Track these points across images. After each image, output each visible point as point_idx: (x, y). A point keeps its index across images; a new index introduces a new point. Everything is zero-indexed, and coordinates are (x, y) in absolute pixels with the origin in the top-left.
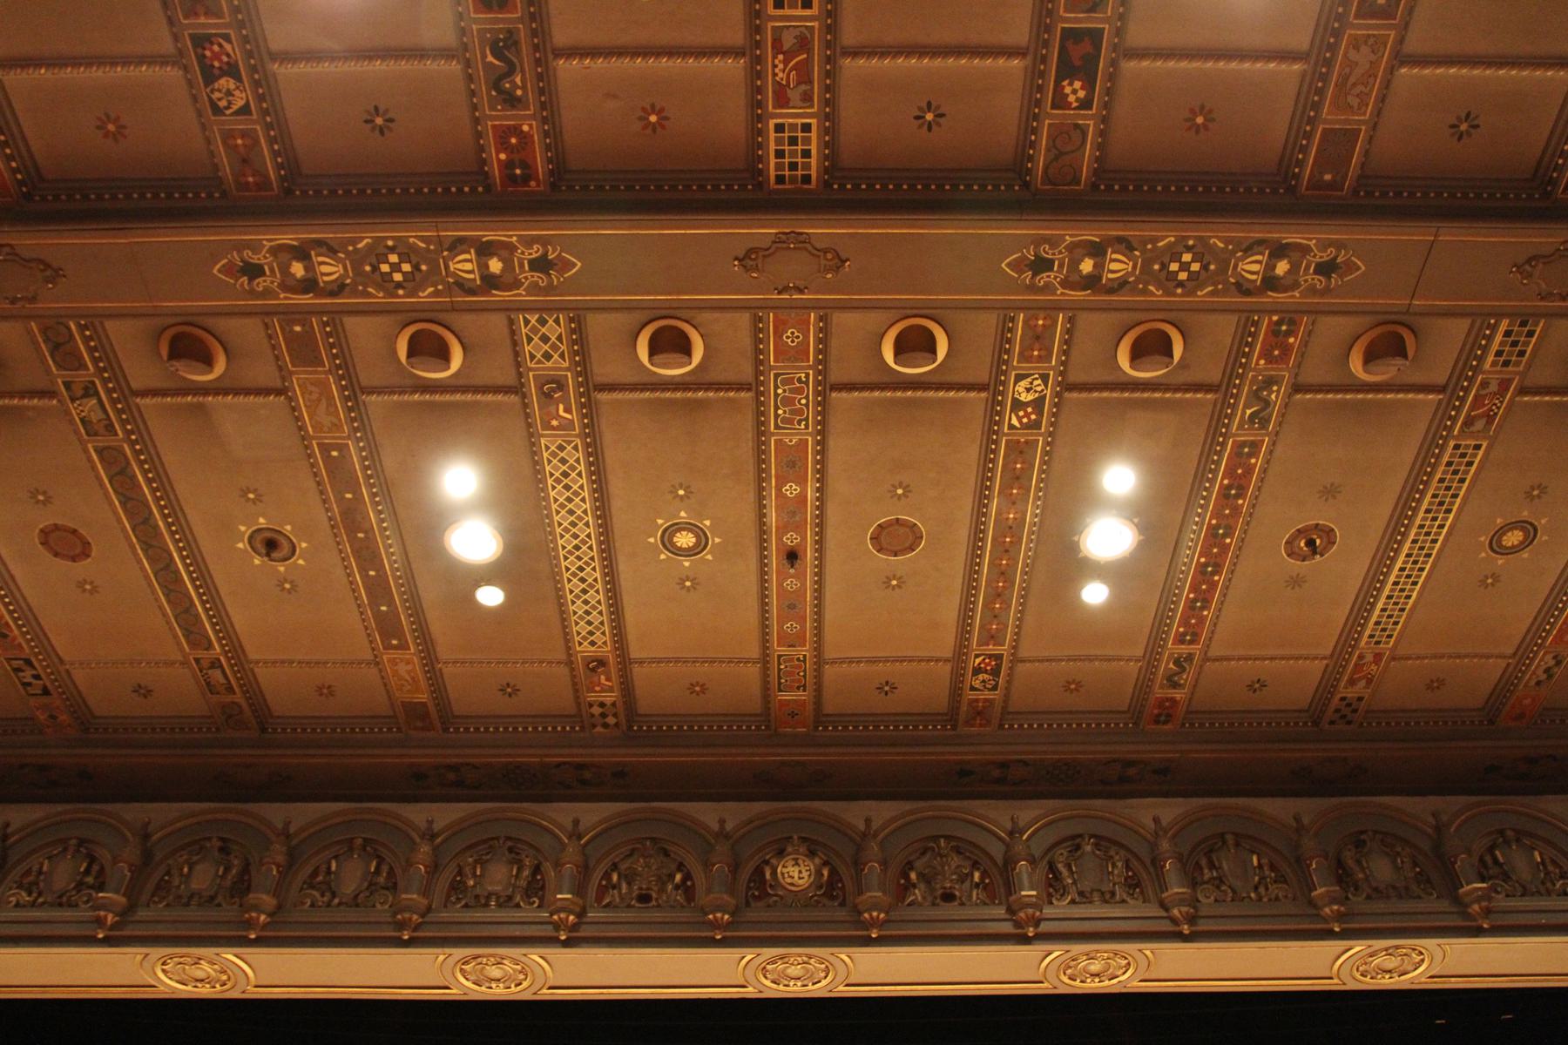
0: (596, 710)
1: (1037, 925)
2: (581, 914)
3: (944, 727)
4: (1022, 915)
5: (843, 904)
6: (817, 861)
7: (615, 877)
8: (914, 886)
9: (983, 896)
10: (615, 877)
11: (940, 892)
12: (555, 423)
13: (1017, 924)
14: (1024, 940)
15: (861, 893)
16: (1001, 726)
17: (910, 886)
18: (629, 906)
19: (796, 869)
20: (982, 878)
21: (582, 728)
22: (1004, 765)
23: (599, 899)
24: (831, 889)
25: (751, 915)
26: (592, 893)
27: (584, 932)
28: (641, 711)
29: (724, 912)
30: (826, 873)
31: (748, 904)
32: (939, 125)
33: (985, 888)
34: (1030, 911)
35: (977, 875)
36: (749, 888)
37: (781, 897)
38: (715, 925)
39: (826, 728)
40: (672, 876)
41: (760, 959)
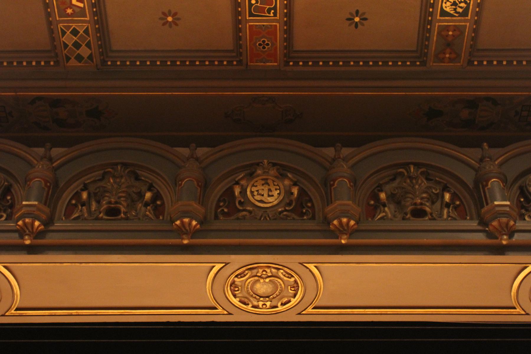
0: (69, 39)
1: (511, 235)
2: (48, 222)
3: (413, 64)
4: (495, 223)
5: (313, 218)
6: (287, 182)
7: (85, 195)
8: (384, 205)
9: (454, 214)
10: (85, 195)
11: (410, 208)
12: (69, 11)
13: (490, 235)
14: (500, 250)
15: (329, 201)
16: (470, 63)
17: (379, 205)
18: (97, 219)
19: (266, 188)
20: (452, 199)
21: (57, 63)
22: (472, 104)
23: (68, 214)
24: (299, 206)
25: (217, 225)
26: (62, 206)
27: (50, 239)
28: (114, 48)
29: (192, 218)
30: (295, 191)
31: (216, 217)
32: (363, 25)
33: (456, 208)
34: (504, 220)
35: (447, 196)
36: (218, 206)
37: (250, 212)
38: (181, 231)
39: (296, 64)
40: (141, 195)
41: (229, 270)
